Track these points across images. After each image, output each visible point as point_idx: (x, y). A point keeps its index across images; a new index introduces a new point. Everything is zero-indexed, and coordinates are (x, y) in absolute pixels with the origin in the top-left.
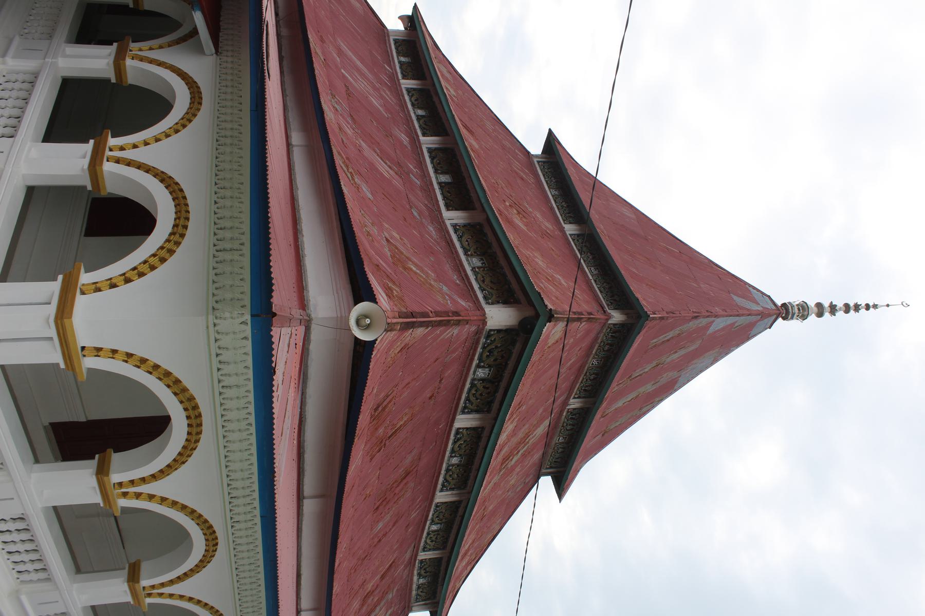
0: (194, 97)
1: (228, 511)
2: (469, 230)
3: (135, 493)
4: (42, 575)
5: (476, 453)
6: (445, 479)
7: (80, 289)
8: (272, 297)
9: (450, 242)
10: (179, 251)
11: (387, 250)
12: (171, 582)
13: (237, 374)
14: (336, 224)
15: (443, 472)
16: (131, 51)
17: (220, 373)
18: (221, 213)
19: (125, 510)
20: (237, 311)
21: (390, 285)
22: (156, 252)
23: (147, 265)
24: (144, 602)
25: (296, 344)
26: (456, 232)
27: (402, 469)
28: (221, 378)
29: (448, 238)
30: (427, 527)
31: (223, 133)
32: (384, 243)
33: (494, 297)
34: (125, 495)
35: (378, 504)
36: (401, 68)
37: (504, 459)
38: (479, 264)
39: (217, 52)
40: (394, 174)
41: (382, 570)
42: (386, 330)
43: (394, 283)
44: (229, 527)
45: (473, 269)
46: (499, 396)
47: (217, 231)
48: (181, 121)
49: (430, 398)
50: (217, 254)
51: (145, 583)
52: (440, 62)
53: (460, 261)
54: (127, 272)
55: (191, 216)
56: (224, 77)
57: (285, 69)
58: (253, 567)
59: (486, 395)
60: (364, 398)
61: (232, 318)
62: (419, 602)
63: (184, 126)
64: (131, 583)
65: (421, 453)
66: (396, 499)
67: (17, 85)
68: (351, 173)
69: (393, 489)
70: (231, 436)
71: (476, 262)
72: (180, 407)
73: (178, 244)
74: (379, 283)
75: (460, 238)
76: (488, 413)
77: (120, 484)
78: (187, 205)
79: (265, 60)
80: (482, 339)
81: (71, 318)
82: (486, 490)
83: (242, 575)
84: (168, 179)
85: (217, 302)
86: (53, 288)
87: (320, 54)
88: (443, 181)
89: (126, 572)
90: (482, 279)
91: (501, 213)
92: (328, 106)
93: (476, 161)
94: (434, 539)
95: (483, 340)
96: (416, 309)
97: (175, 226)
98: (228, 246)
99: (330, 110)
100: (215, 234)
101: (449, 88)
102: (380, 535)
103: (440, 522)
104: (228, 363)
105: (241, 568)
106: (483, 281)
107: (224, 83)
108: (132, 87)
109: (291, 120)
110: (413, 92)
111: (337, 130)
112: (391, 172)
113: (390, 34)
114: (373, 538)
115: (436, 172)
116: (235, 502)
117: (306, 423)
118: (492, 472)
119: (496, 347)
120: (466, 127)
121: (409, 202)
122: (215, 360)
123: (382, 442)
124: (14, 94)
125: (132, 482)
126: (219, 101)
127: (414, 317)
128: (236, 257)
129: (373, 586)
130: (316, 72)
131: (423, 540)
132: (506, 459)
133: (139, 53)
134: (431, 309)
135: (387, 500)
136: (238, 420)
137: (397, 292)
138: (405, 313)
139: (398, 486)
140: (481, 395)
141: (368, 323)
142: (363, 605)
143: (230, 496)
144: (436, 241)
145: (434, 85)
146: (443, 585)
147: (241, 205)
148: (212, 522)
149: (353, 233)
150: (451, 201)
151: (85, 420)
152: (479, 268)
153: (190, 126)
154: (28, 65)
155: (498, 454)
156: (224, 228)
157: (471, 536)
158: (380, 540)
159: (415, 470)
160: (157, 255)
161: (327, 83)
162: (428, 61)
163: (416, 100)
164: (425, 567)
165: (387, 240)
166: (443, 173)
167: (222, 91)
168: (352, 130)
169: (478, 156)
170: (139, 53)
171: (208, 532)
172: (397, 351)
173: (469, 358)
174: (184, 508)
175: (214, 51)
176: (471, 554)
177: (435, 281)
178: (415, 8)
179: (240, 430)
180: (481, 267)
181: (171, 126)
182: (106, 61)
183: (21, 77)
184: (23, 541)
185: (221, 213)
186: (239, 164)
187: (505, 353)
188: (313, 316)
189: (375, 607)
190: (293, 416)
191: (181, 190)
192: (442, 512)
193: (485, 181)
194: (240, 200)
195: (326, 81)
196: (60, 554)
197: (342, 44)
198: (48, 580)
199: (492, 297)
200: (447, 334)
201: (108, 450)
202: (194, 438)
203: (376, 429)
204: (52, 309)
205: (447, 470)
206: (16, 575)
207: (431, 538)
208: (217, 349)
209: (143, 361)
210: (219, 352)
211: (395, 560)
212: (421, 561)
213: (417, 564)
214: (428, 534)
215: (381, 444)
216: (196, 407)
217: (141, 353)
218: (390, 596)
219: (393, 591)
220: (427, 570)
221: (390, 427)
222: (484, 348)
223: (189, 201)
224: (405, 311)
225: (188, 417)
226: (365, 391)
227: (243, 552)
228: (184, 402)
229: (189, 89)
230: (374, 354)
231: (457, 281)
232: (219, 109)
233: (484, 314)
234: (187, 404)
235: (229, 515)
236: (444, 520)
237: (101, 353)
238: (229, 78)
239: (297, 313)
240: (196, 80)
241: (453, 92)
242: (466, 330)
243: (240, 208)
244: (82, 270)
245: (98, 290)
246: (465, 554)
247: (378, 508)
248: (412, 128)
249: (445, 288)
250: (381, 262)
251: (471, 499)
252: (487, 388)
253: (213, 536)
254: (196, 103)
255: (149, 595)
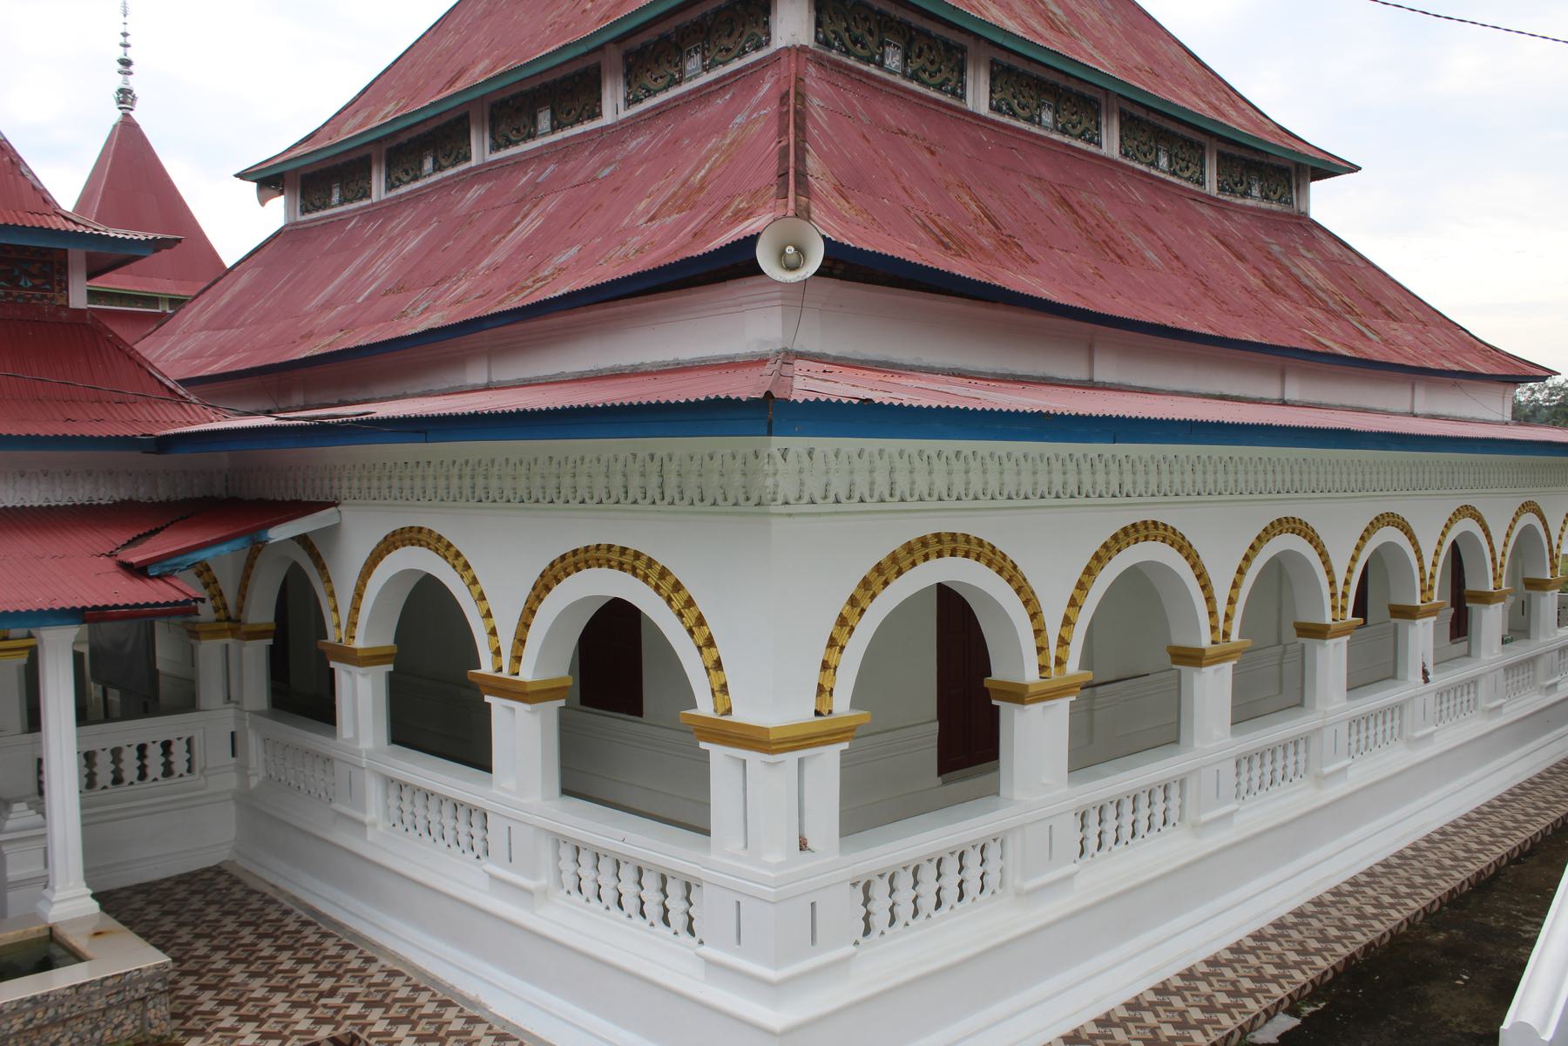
0: (410, 540)
1: (1101, 501)
2: (636, 77)
3: (1058, 646)
4: (1174, 791)
5: (1037, 78)
6: (1079, 137)
7: (722, 715)
8: (738, 400)
9: (657, 112)
10: (662, 560)
11: (669, 220)
12: (1209, 599)
13: (872, 471)
14: (622, 307)
15: (1066, 140)
16: (340, 641)
17: (867, 498)
18: (600, 492)
19: (1087, 661)
20: (763, 466)
21: (729, 213)
22: (664, 598)
23: (685, 612)
24: (1236, 644)
25: (825, 371)
26: (640, 101)
27: (1055, 210)
28: (876, 497)
29: (649, 115)
30: (1162, 176)
31: (467, 491)
32: (656, 224)
33: (756, 31)
34: (1060, 662)
35: (1112, 256)
36: (351, 201)
37: (1052, 28)
38: (697, 58)
39: (334, 504)
40: (538, 208)
41: (1229, 257)
42: (809, 219)
43: (726, 207)
44: (1128, 500)
45: (706, 69)
46: (936, 29)
47: (631, 499)
48: (450, 559)
49: (933, 153)
50: (667, 499)
51: (1205, 641)
52: (337, 131)
53: (691, 92)
54: (695, 642)
55: (604, 541)
56: (374, 492)
57: (360, 397)
58: (1199, 468)
59: (934, 52)
60: (924, 264)
61: (775, 474)
62: (1292, 198)
63: (458, 555)
64: (1204, 662)
65: (1029, 176)
66: (1107, 225)
67: (406, 807)
68: (534, 282)
69: (1090, 229)
70: (976, 486)
71: (694, 64)
72: (922, 567)
73: (651, 563)
74: (725, 232)
75: (650, 93)
76: (966, 51)
77: (1042, 668)
78: (587, 549)
79: (340, 420)
80: (831, 55)
81: (767, 729)
82: (1106, 63)
83: (1210, 486)
84: (545, 580)
85: (748, 499)
86: (719, 755)
87: (331, 338)
88: (548, 123)
89: (1184, 669)
90: (724, 53)
91: (606, 17)
92: (421, 322)
93: (513, 63)
94: (1183, 164)
95: (834, 54)
96: (772, 168)
97: (621, 567)
98: (654, 481)
99: (427, 318)
100: (635, 502)
101: (382, 114)
102: (1167, 255)
103: (1154, 150)
104: (852, 484)
105: (1199, 486)
106: (728, 50)
107: (385, 492)
108: (400, 636)
109: (446, 386)
110: (393, 178)
111: (460, 307)
112: (533, 214)
113: (292, 220)
114: (1172, 269)
115: (532, 136)
116: (1086, 487)
117: (964, 367)
118: (1072, 50)
119: (847, 29)
120: (452, 82)
121: (585, 183)
122: (845, 506)
123: (1005, 242)
124: (420, 811)
125: (1040, 650)
126: (415, 498)
127: (788, 173)
128: (674, 466)
129: (1254, 275)
130: (362, 343)
131: (1184, 183)
132: (1051, 23)
133: (343, 627)
134: (774, 144)
135: (1107, 240)
136: (950, 473)
137: (742, 201)
138: (779, 187)
139: (1084, 219)
140: (932, 62)
141: (793, 249)
142: (1286, 296)
143: (1077, 495)
144: (656, 134)
145: (378, 141)
146: (1267, 153)
147: (587, 460)
148: (1117, 529)
149: (638, 276)
150: (584, 108)
151: (937, 723)
152: (704, 60)
153: (458, 545)
154: (374, 792)
155: (1042, 37)
156: (626, 487)
157: (1185, 97)
158: (1177, 257)
159: (1059, 189)
160: (669, 595)
161: (381, 325)
162: (336, 151)
163: (407, 174)
164: (1232, 185)
165: (652, 219)
166: (534, 121)
167: (398, 495)
168: (461, 283)
169: (504, 59)
170: (343, 627)
171: (1133, 536)
172: (846, 204)
173: (864, 80)
174: (1089, 571)
175: (332, 509)
176: (1218, 99)
177: (725, 136)
178: (242, 176)
179: (967, 472)
180: (703, 53)
181: (458, 576)
182: (360, 679)
183: (394, 802)
184: (1118, 815)
185: (600, 492)
186: (518, 464)
187: (859, 14)
188: (779, 347)
189: (1291, 274)
190: (948, 383)
191: (563, 558)
192: (1137, 147)
193: (547, 46)
194: (579, 462)
195: (377, 327)
196: (1142, 765)
197: (314, 303)
198: (1182, 783)
199: (757, 35)
200: (820, 116)
201: (985, 685)
202: (975, 548)
203: (981, 249)
204: (754, 758)
205: (1064, 131)
206: (1169, 827)
207: (1181, 170)
208: (827, 501)
209: (842, 621)
210: (832, 498)
211: (1213, 235)
212: (1221, 189)
213: (1225, 198)
214: (1174, 174)
215: (1007, 243)
216: (923, 542)
217: (828, 626)
218: (1276, 249)
219: (1268, 243)
220: (1237, 179)
221: (980, 225)
222: (848, 53)
223: (581, 545)
224: (776, 187)
225: (940, 555)
226: (913, 261)
227: (1171, 482)
228: (914, 560)
229: (396, 548)
230: (849, 243)
231: (727, 97)
232: (428, 498)
233: (787, 49)
234: (918, 555)
235: (1108, 500)
236: (1152, 144)
237: (827, 687)
238: (375, 483)
239: (769, 369)
240: (381, 538)
241: (388, 109)
242: (814, 84)
243: (591, 461)
244: (692, 712)
245: (724, 688)
246: (1216, 109)
247: (1120, 257)
248: (456, 179)
249: (739, 120)
250: (688, 229)
251: (1118, 90)
252: (921, 50)
253: (1142, 528)
254: (419, 536)
255: (1226, 635)
